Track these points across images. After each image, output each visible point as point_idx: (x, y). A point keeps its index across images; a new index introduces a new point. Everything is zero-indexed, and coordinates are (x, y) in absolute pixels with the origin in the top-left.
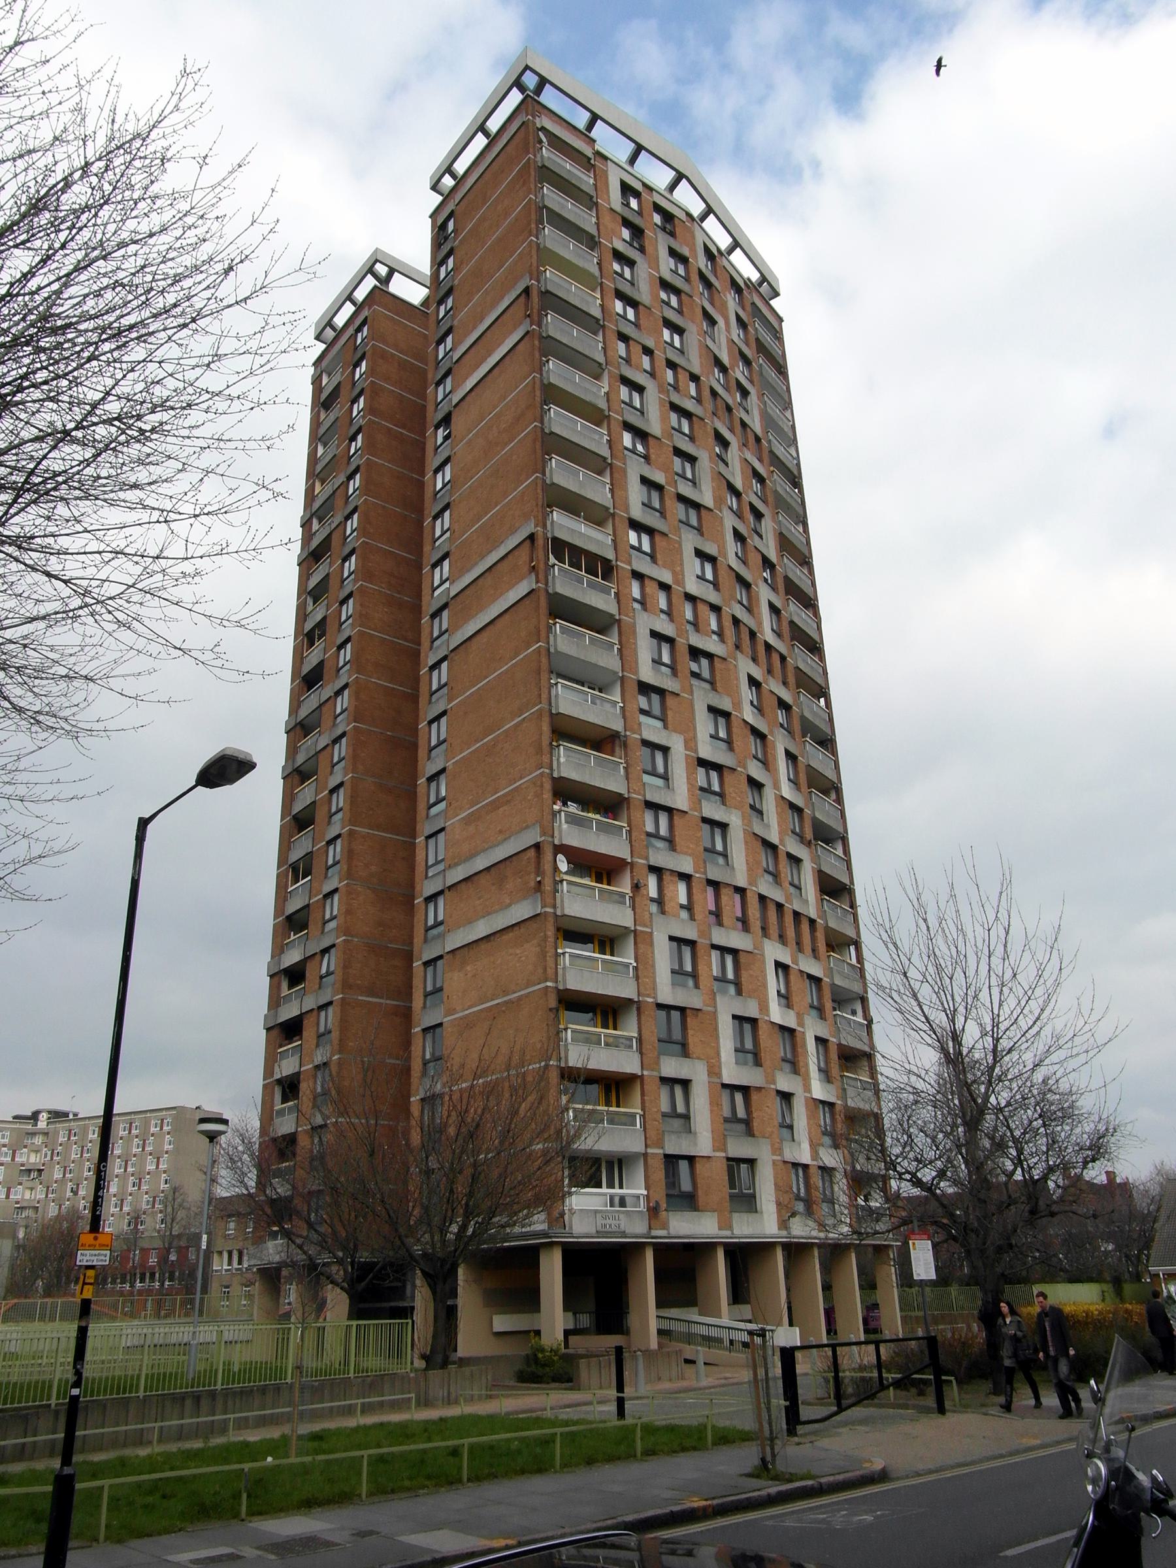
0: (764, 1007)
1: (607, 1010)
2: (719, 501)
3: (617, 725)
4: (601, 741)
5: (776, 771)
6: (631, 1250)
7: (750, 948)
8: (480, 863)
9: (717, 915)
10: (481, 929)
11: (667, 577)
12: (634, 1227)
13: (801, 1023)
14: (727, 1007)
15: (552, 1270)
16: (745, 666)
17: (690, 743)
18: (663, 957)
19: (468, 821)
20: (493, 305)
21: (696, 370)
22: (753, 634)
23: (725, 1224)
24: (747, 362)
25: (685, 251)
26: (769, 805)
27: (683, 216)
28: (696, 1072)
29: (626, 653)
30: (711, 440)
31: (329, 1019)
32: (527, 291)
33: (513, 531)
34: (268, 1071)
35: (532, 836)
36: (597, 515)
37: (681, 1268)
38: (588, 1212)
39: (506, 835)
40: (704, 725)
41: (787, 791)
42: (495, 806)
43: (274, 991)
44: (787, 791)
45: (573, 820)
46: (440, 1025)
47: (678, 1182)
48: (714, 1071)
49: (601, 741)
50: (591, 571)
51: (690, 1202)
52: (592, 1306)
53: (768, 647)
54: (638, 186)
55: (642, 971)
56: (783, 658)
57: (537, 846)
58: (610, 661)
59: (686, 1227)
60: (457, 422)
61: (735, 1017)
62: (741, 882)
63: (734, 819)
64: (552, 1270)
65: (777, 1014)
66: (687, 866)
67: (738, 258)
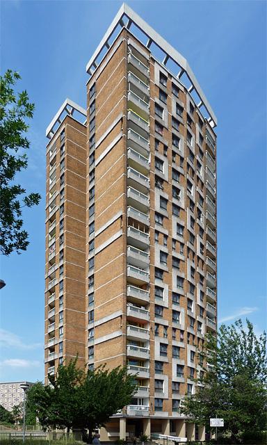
0: (186, 362)
1: (142, 362)
2: (186, 206)
3: (148, 281)
4: (144, 286)
5: (196, 296)
6: (145, 420)
7: (183, 346)
8: (105, 320)
9: (174, 337)
10: (105, 339)
11: (166, 233)
12: (146, 415)
13: (196, 367)
14: (175, 362)
15: (123, 424)
16: (189, 264)
17: (170, 287)
18: (157, 349)
19: (101, 308)
20: (110, 125)
21: (183, 155)
22: (194, 254)
23: (170, 414)
24: (202, 153)
25: (182, 105)
26: (193, 307)
27: (183, 89)
28: (165, 378)
29: (152, 258)
30: (186, 183)
31: (63, 330)
32: (122, 119)
33: (115, 214)
34: (46, 302)
35: (120, 313)
36: (145, 210)
37: (158, 425)
38: (131, 411)
39: (112, 312)
40: (175, 282)
41: (199, 303)
42: (109, 304)
43: (46, 353)
44: (199, 303)
45: (131, 328)
46: (93, 364)
47: (159, 404)
48: (170, 378)
49: (144, 286)
50: (141, 229)
51: (159, 409)
52: (134, 431)
53: (199, 258)
54: (166, 75)
55: (152, 352)
56: (203, 262)
57: (121, 316)
58: (146, 260)
59: (158, 414)
60: (97, 174)
61: (178, 276)
62: (183, 329)
63: (182, 311)
64: (123, 424)
65: (189, 364)
66: (166, 323)
67: (202, 110)
